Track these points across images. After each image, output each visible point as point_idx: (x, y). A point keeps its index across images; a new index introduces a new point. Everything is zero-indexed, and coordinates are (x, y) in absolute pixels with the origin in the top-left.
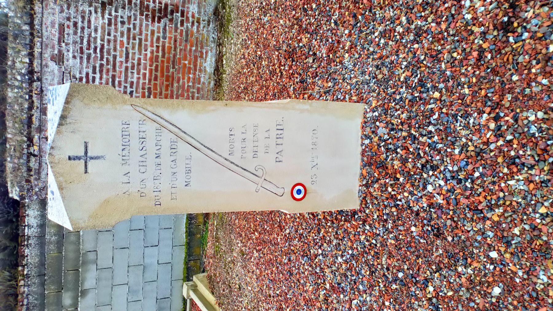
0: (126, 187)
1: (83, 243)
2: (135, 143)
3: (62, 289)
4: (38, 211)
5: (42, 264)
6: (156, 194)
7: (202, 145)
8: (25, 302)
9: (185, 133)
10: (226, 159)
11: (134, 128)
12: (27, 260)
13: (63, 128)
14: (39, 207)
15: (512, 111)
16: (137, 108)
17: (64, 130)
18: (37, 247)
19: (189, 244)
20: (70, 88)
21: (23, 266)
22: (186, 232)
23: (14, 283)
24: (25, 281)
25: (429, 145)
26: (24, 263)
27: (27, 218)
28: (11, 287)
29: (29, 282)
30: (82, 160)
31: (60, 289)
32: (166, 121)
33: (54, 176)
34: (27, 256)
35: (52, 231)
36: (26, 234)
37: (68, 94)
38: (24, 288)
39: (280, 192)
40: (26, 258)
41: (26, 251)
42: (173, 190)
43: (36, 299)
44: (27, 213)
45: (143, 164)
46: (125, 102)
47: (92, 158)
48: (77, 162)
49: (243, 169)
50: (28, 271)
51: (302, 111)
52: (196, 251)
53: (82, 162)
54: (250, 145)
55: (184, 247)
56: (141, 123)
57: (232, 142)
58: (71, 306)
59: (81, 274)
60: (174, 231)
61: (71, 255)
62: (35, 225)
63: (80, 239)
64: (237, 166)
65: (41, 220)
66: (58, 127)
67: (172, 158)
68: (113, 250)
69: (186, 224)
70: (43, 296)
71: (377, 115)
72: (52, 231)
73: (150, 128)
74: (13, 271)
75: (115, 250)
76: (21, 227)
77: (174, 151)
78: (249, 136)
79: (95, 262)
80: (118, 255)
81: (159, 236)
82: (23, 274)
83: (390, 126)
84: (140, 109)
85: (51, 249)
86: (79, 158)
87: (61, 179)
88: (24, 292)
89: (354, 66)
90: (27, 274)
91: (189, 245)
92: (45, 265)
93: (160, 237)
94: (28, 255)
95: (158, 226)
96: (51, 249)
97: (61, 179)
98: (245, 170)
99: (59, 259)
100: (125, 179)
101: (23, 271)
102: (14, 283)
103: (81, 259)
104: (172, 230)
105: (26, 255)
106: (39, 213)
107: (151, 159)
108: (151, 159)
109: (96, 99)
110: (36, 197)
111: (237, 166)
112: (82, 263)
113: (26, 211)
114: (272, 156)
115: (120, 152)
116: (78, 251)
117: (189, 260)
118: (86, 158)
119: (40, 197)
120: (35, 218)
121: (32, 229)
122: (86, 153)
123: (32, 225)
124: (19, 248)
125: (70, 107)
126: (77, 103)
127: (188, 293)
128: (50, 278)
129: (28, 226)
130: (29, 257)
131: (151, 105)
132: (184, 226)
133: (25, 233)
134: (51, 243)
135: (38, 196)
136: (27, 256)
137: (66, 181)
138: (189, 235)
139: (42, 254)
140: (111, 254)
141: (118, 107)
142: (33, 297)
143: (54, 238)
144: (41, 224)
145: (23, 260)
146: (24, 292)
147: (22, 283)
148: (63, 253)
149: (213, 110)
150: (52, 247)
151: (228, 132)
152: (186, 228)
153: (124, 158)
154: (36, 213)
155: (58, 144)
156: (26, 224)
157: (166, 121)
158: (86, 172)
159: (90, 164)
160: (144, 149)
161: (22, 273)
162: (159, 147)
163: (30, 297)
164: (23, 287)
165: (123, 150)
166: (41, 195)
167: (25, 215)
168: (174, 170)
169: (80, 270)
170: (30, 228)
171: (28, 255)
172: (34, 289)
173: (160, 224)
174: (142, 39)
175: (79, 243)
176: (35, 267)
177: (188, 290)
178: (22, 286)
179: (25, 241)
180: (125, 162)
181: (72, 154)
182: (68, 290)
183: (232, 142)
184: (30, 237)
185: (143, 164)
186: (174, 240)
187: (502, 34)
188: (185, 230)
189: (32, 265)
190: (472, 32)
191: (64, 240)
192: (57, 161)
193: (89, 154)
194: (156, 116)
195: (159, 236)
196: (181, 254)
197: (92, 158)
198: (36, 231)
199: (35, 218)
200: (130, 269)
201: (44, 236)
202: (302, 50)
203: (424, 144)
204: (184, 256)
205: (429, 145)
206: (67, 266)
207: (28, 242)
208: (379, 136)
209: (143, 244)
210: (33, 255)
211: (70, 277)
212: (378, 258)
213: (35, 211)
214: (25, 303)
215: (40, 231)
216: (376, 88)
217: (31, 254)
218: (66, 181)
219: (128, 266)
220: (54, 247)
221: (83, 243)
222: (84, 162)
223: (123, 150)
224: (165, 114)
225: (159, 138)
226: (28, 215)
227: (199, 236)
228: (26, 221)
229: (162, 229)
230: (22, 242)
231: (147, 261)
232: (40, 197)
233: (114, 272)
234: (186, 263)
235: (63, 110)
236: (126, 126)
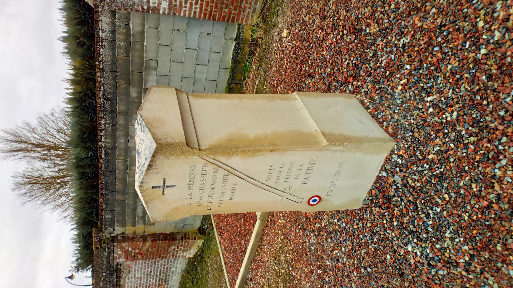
0: (188, 201)
1: (146, 52)
2: (198, 178)
3: (130, 85)
4: (109, 19)
5: (114, 63)
6: (208, 204)
7: (247, 176)
8: (102, 89)
9: (235, 170)
10: (263, 184)
11: (199, 169)
12: (102, 57)
13: (150, 172)
14: (110, 15)
15: (483, 265)
16: (203, 157)
17: (150, 173)
18: (110, 49)
19: (233, 70)
20: (156, 148)
21: (100, 62)
22: (233, 58)
23: (93, 71)
24: (101, 74)
25: (424, 222)
26: (100, 59)
27: (100, 23)
28: (90, 73)
29: (104, 75)
30: (161, 188)
31: (128, 84)
32: (223, 163)
34: (102, 55)
35: (121, 37)
36: (100, 36)
37: (154, 152)
38: (101, 78)
39: (299, 200)
40: (101, 56)
41: (101, 50)
42: (221, 202)
43: (110, 88)
44: (100, 18)
45: (202, 188)
46: (194, 154)
47: (168, 187)
48: (158, 189)
49: (274, 188)
50: (104, 66)
51: (335, 151)
52: (239, 76)
53: (161, 189)
54: (284, 175)
55: (229, 70)
56: (204, 165)
57: (270, 174)
58: (137, 98)
59: (145, 76)
60: (222, 55)
61: (137, 60)
62: (108, 30)
63: (144, 48)
64: (271, 187)
65: (112, 26)
66: (146, 171)
67: (223, 185)
68: (170, 62)
70: (115, 87)
71: (400, 162)
72: (121, 37)
73: (211, 168)
74: (91, 61)
75: (172, 62)
76: (96, 30)
77: (225, 180)
78: (286, 169)
79: (156, 69)
80: (174, 66)
81: (209, 58)
82: (100, 68)
83: (405, 181)
84: (205, 158)
85: (121, 52)
86: (159, 187)
87: (147, 198)
88: (101, 81)
89: (402, 103)
90: (102, 68)
91: (233, 71)
92: (116, 64)
94: (102, 53)
95: (209, 49)
96: (121, 52)
97: (147, 198)
98: (276, 189)
99: (127, 61)
100: (189, 197)
101: (99, 65)
102: (93, 71)
103: (144, 64)
104: (221, 55)
105: (101, 53)
106: (110, 20)
107: (208, 186)
108: (208, 186)
109: (174, 154)
110: (108, 8)
111: (271, 187)
112: (145, 68)
113: (99, 17)
114: (300, 181)
115: (187, 183)
116: (142, 57)
117: (232, 83)
118: (164, 186)
119: (111, 8)
120: (107, 24)
121: (105, 33)
122: (164, 183)
123: (105, 29)
124: (96, 46)
125: (155, 159)
126: (160, 157)
128: (120, 75)
129: (102, 30)
130: (103, 56)
131: (213, 155)
132: (232, 53)
133: (99, 36)
134: (121, 47)
135: (109, 7)
136: (102, 55)
137: (150, 199)
138: (235, 63)
139: (114, 55)
140: (169, 65)
141: (189, 157)
142: (108, 86)
143: (122, 44)
144: (112, 30)
145: (99, 57)
146: (101, 81)
147: (99, 74)
148: (130, 57)
149: (261, 155)
150: (121, 51)
151: (269, 167)
152: (233, 55)
153: (189, 186)
154: (108, 20)
155: (146, 180)
156: (100, 28)
157: (223, 163)
158: (163, 194)
159: (166, 190)
160: (204, 180)
161: (98, 67)
162: (215, 179)
163: (106, 86)
164: (99, 77)
165: (189, 181)
166: (112, 7)
167: (98, 19)
168: (223, 191)
169: (144, 73)
170: (104, 32)
171: (102, 53)
172: (108, 80)
174: (213, 6)
175: (143, 51)
176: (108, 65)
178: (99, 76)
179: (99, 42)
180: (190, 188)
181: (154, 185)
182: (134, 86)
183: (270, 174)
184: (104, 39)
185: (202, 188)
187: (510, 213)
188: (231, 56)
189: (106, 62)
190: (493, 187)
191: (131, 47)
192: (144, 189)
193: (166, 184)
194: (215, 161)
195: (209, 58)
196: (226, 76)
197: (168, 187)
198: (108, 35)
199: (107, 24)
200: (184, 79)
201: (115, 41)
202: (366, 38)
203: (421, 218)
204: (228, 78)
205: (424, 222)
206: (134, 67)
207: (102, 43)
208: (394, 179)
209: (195, 61)
210: (107, 54)
211: (136, 76)
212: (360, 247)
213: (107, 18)
214: (102, 89)
215: (111, 36)
216: (409, 140)
217: (105, 53)
218: (150, 199)
219: (182, 77)
220: (124, 51)
221: (146, 52)
222: (162, 189)
223: (189, 181)
224: (223, 159)
225: (215, 174)
226: (101, 21)
227: (243, 65)
228: (100, 25)
230: (97, 42)
231: (198, 76)
232: (111, 8)
234: (229, 84)
235: (150, 162)
236: (193, 168)
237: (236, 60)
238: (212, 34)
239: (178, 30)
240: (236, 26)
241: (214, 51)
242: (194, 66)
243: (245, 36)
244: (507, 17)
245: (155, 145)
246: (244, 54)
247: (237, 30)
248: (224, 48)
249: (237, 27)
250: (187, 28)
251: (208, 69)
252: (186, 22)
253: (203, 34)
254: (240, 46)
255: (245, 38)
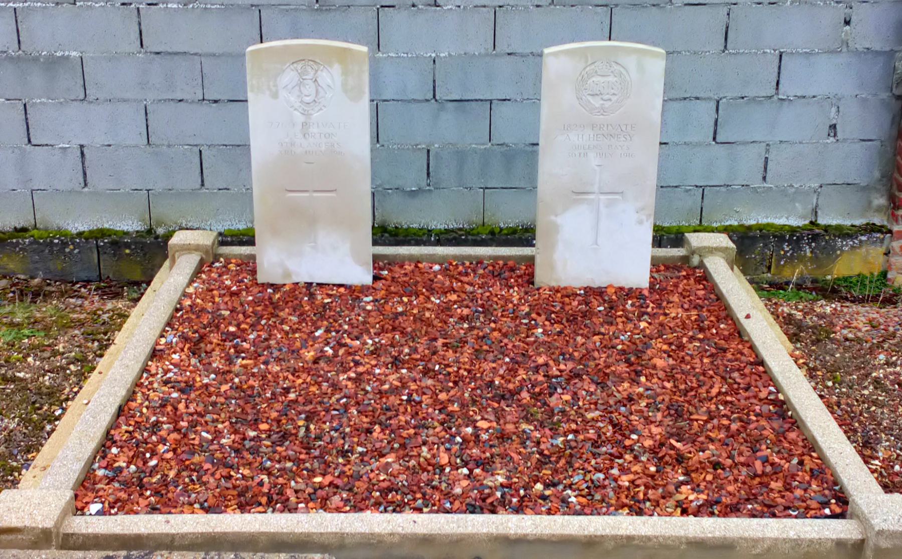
33: (804, 516)
69: (768, 225)
75: (725, 10)
81: (745, 143)
93: (740, 148)
95: (778, 139)
104: (757, 183)
127: (187, 249)
173: (784, 145)
177: (197, 248)
186: (723, 189)
195: (745, 143)
204: (666, 225)
229: (767, 151)
233: (654, 8)
237: (754, 239)
238: (832, 139)
239: (847, 23)
240: (862, 216)
241: (771, 157)
242: (711, 95)
243: (845, 255)
244: (179, 399)
245: (278, 79)
246: (778, 265)
247: (848, 223)
248: (783, 192)
249: (857, 222)
250: (857, 53)
251: (698, 144)
252: (877, 47)
253: (834, 110)
254: (809, 244)
255: (838, 256)
